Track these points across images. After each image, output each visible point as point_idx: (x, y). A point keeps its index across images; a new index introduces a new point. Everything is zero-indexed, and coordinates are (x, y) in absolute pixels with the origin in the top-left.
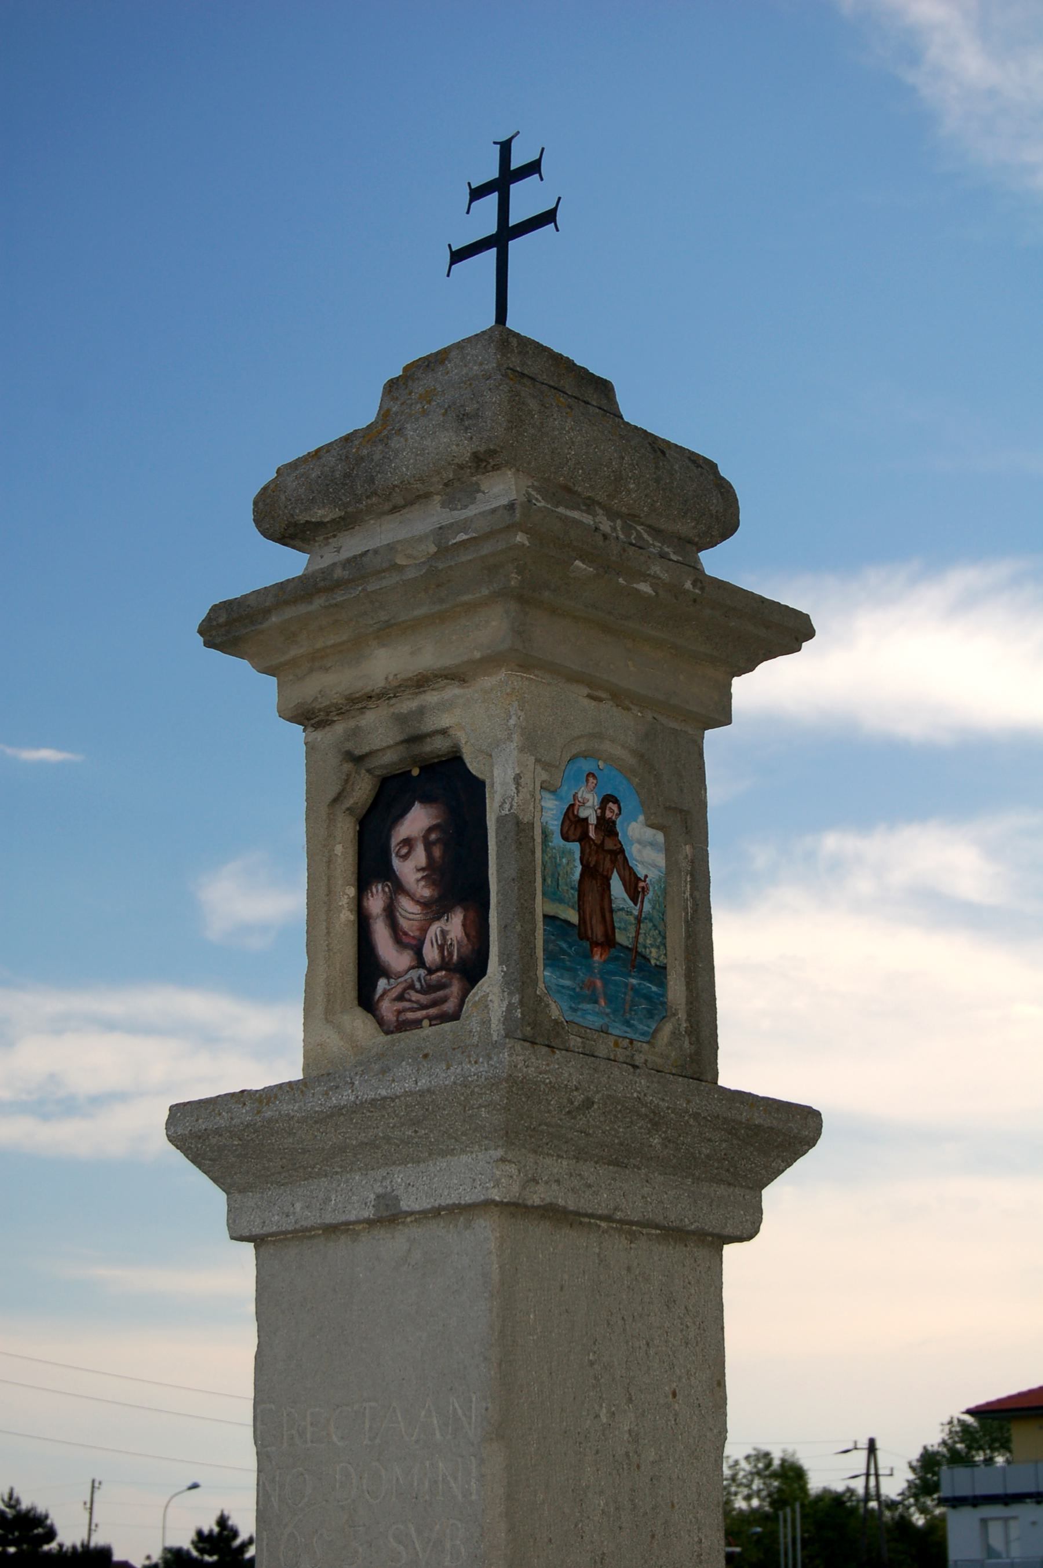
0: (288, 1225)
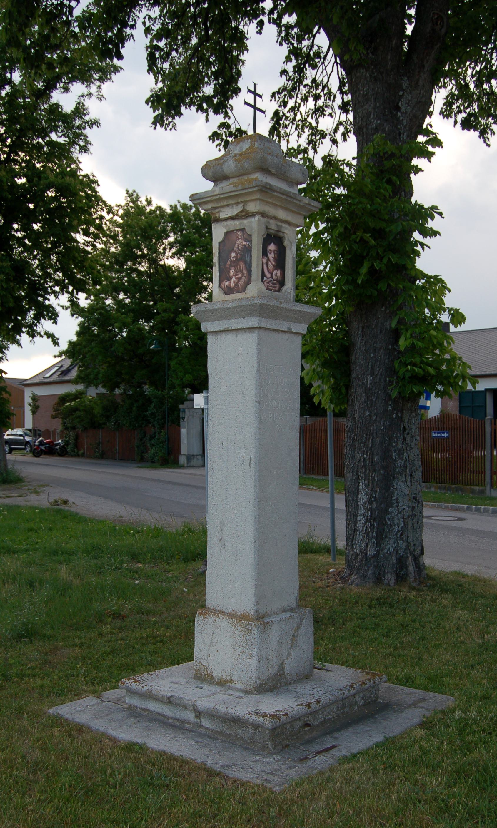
0: (271, 327)
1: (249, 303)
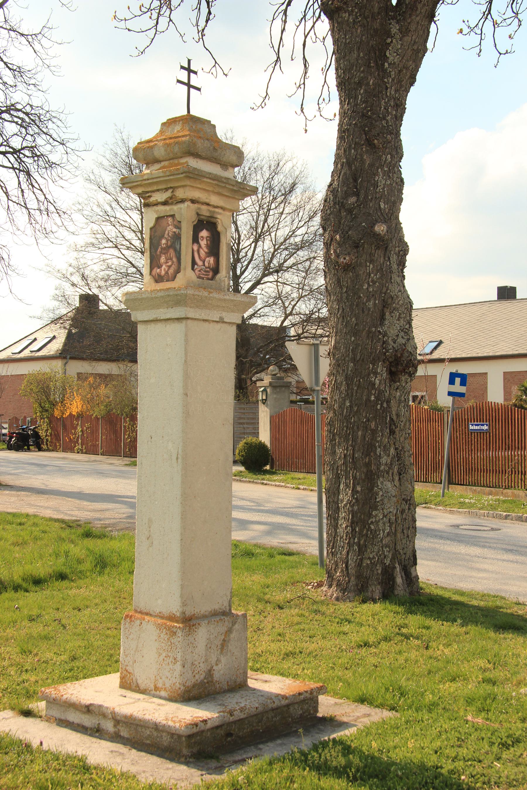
0: (201, 318)
1: (176, 293)
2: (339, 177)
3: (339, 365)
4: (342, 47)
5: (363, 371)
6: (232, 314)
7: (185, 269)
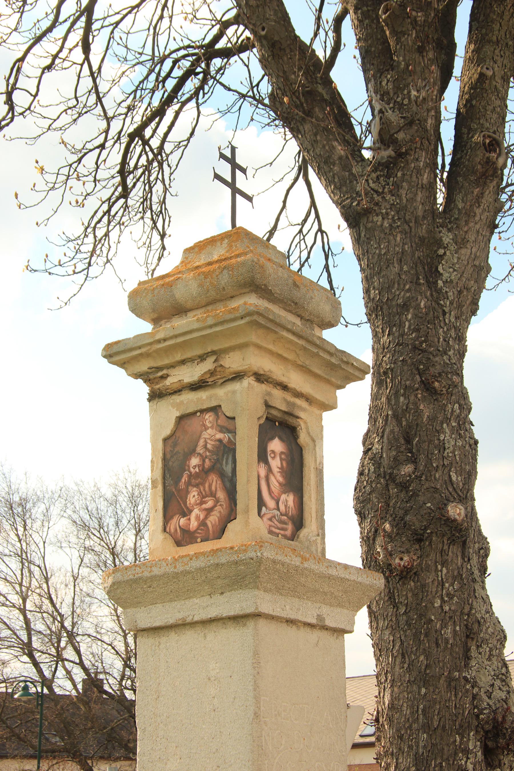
0: (283, 614)
1: (235, 557)
2: (382, 437)
3: (401, 737)
4: (375, 261)
5: (446, 748)
6: (339, 610)
7: (247, 511)
